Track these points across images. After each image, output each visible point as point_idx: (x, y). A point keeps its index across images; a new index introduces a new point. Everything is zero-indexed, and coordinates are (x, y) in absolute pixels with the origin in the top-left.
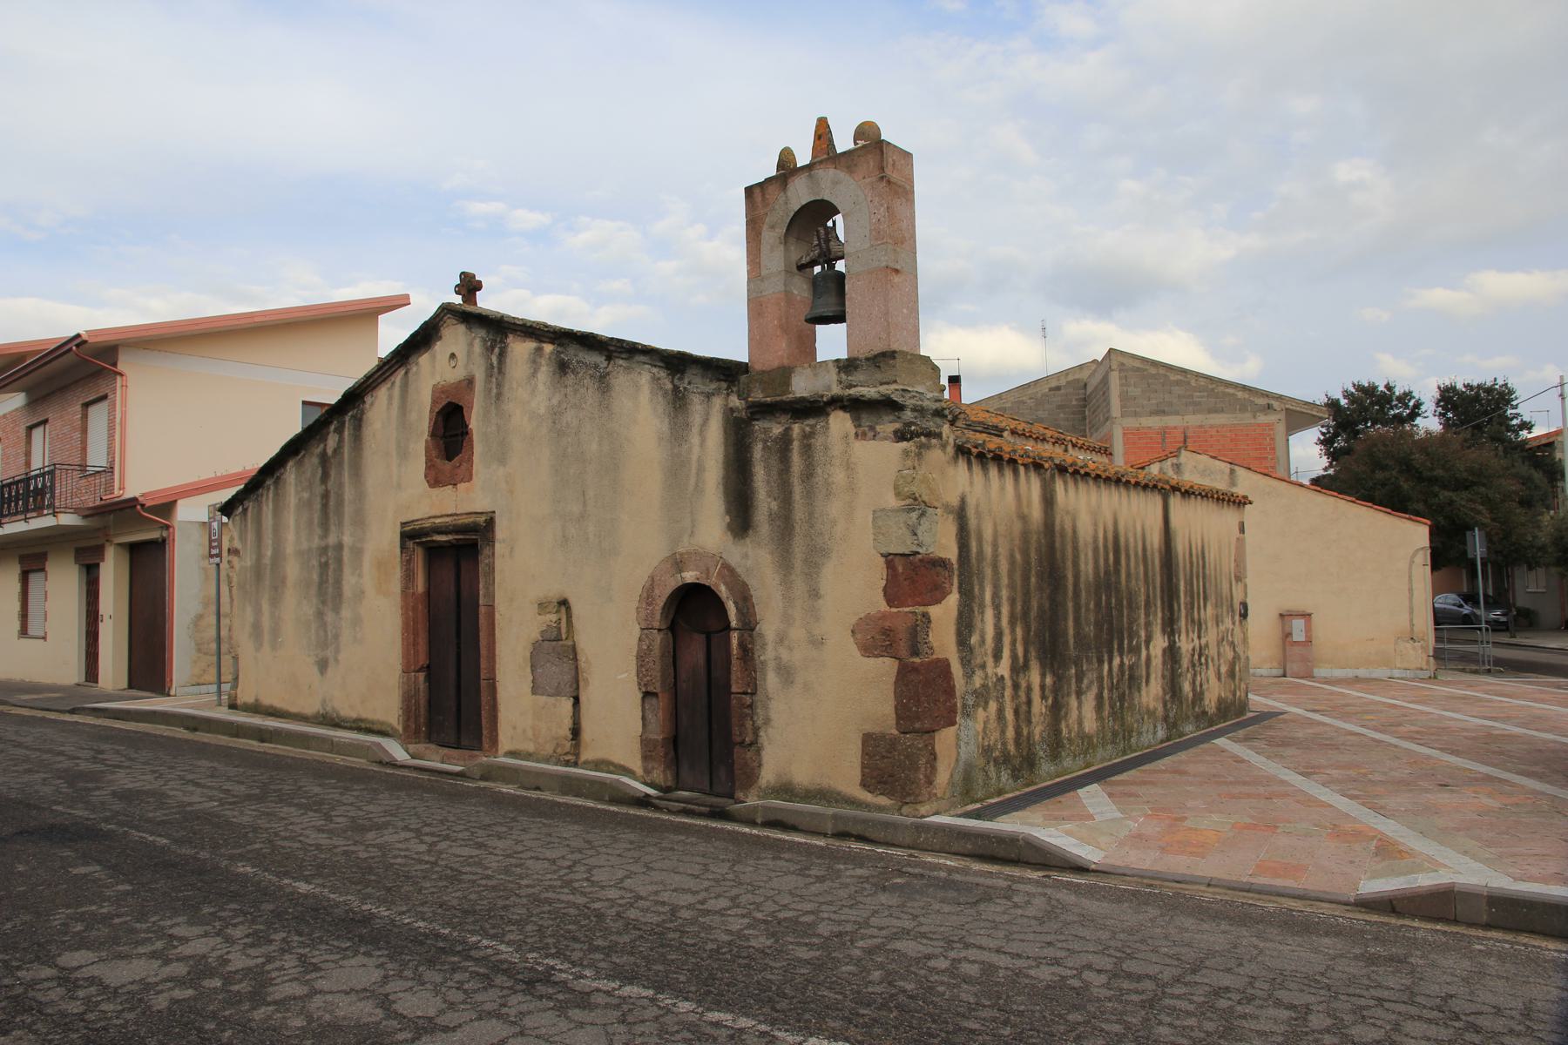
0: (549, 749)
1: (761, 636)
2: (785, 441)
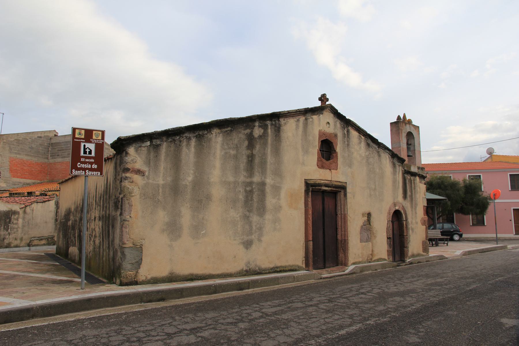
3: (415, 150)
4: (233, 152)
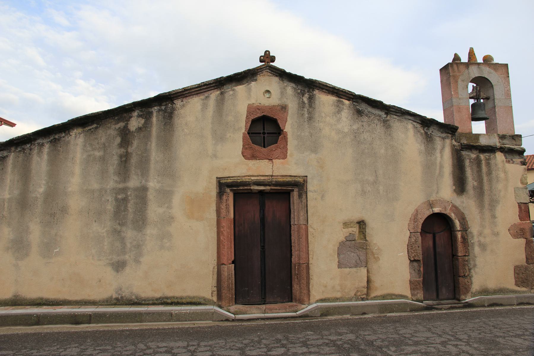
0: (352, 294)
1: (471, 233)
2: (478, 162)
3: (495, 107)
4: (98, 154)
